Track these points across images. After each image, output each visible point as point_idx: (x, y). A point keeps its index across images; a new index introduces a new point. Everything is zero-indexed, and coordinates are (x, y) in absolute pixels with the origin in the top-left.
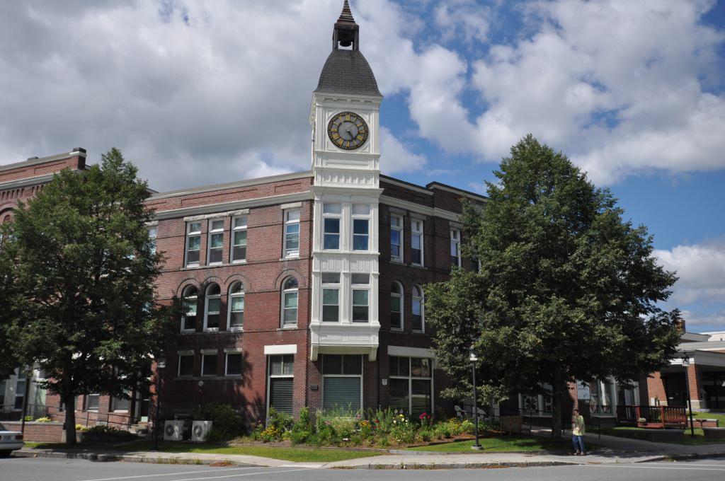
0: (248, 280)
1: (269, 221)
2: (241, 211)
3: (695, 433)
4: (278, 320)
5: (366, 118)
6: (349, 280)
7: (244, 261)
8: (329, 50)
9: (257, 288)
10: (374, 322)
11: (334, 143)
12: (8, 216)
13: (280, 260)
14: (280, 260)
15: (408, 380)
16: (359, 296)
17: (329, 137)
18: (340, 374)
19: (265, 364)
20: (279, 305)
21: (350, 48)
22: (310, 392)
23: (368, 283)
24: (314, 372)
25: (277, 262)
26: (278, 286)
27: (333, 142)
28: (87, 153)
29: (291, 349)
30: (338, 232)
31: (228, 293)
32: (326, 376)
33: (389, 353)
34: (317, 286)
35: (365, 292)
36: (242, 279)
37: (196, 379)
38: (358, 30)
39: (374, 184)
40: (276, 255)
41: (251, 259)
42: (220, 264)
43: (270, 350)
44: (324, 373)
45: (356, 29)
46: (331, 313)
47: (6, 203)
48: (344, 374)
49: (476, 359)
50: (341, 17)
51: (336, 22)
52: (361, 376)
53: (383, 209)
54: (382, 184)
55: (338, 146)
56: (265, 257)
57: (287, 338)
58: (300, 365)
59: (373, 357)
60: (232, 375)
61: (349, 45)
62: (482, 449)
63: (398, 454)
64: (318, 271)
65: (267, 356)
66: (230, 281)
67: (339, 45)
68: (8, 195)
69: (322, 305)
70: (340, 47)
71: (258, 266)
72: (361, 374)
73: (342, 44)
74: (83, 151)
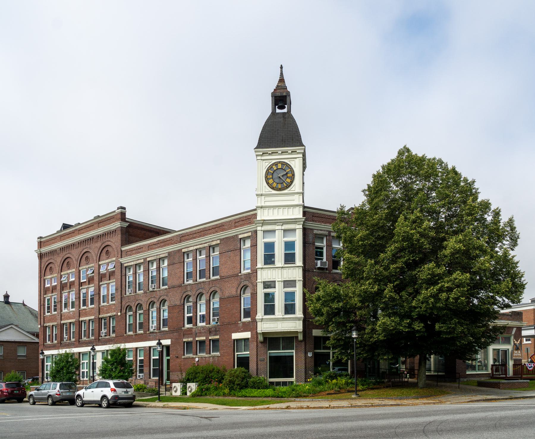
0: (221, 290)
1: (232, 248)
2: (215, 242)
3: (457, 374)
4: (239, 316)
5: (292, 163)
6: (282, 284)
7: (218, 277)
8: (269, 111)
9: (227, 294)
10: (299, 313)
11: (294, 177)
12: (51, 267)
13: (239, 274)
14: (239, 274)
15: (330, 352)
16: (289, 297)
17: (266, 182)
18: (280, 350)
19: (233, 346)
20: (239, 306)
21: (285, 110)
22: (259, 363)
23: (295, 287)
24: (262, 349)
25: (237, 275)
26: (239, 292)
27: (269, 186)
28: (126, 209)
29: (247, 335)
30: (294, 250)
31: (210, 299)
32: (270, 352)
33: (250, 332)
34: (261, 292)
35: (293, 294)
36: (217, 289)
37: (194, 356)
38: (290, 95)
39: (298, 214)
40: (236, 271)
41: (223, 275)
42: (204, 280)
43: (236, 336)
44: (269, 350)
45: (288, 94)
46: (270, 309)
47: (85, 248)
48: (283, 350)
49: (357, 336)
50: (278, 86)
51: (273, 91)
52: (294, 351)
53: (305, 230)
54: (304, 213)
55: (273, 188)
56: (231, 273)
57: (245, 328)
58: (253, 345)
59: (301, 337)
60: (214, 354)
61: (284, 108)
62: (360, 396)
63: (300, 401)
64: (280, 280)
65: (234, 340)
66: (210, 291)
67: (277, 109)
68: (101, 237)
69: (284, 303)
70: (278, 111)
71: (226, 279)
72: (294, 349)
73: (279, 108)
74: (124, 208)
